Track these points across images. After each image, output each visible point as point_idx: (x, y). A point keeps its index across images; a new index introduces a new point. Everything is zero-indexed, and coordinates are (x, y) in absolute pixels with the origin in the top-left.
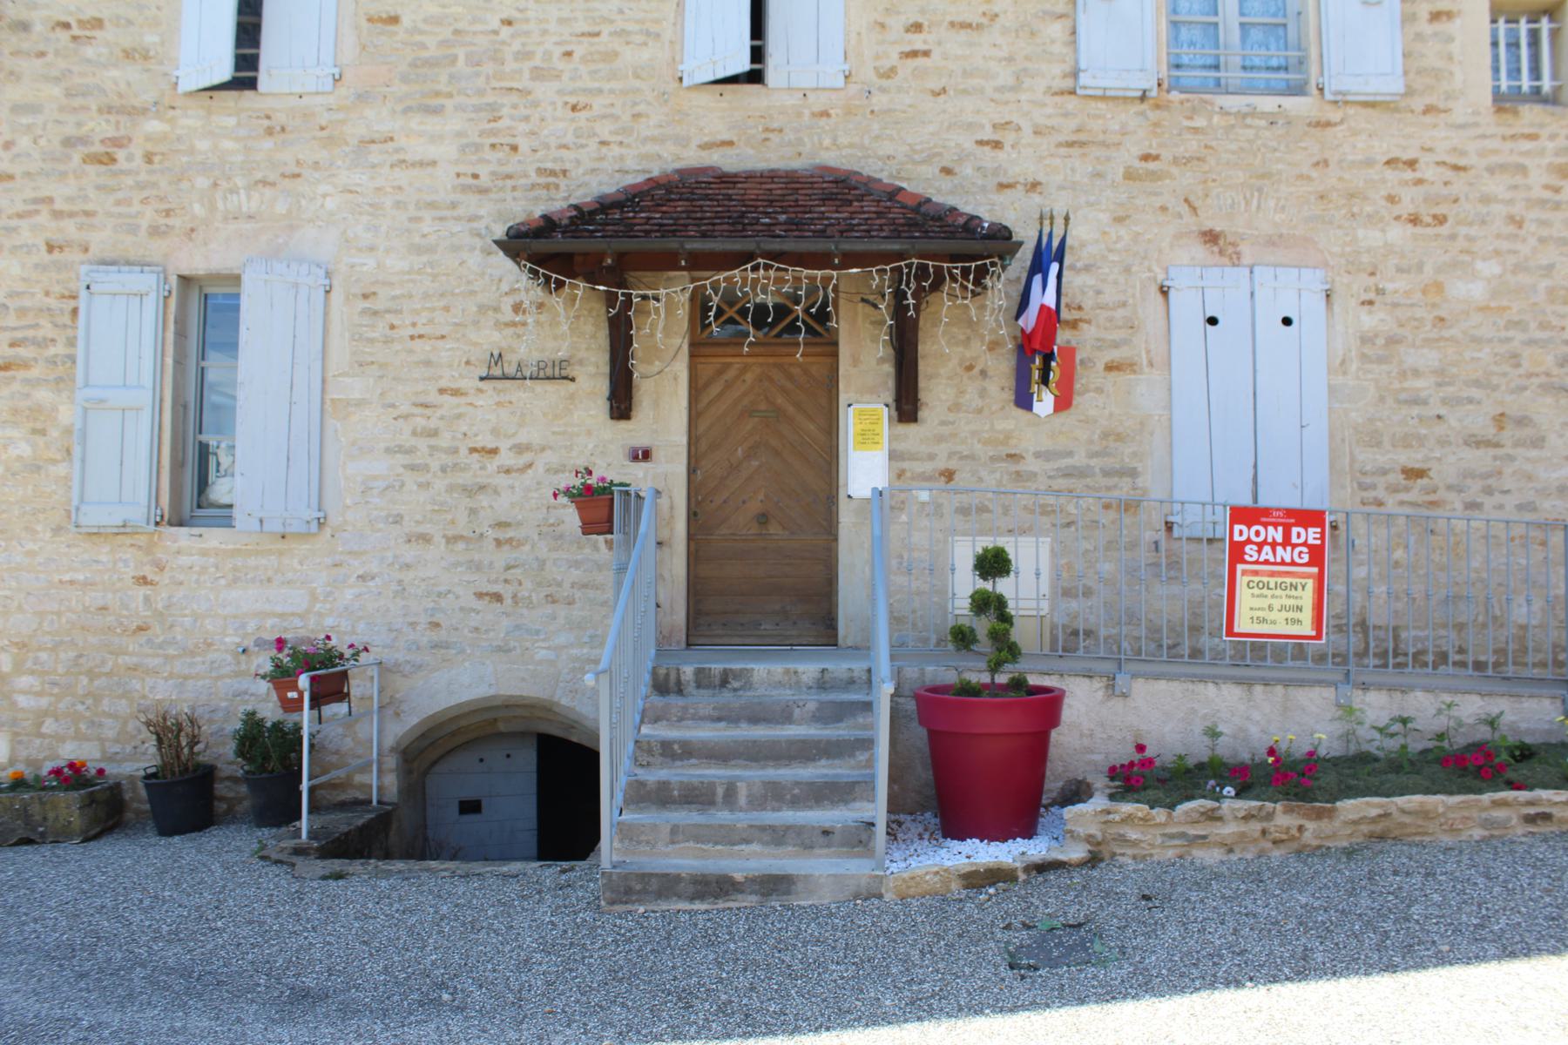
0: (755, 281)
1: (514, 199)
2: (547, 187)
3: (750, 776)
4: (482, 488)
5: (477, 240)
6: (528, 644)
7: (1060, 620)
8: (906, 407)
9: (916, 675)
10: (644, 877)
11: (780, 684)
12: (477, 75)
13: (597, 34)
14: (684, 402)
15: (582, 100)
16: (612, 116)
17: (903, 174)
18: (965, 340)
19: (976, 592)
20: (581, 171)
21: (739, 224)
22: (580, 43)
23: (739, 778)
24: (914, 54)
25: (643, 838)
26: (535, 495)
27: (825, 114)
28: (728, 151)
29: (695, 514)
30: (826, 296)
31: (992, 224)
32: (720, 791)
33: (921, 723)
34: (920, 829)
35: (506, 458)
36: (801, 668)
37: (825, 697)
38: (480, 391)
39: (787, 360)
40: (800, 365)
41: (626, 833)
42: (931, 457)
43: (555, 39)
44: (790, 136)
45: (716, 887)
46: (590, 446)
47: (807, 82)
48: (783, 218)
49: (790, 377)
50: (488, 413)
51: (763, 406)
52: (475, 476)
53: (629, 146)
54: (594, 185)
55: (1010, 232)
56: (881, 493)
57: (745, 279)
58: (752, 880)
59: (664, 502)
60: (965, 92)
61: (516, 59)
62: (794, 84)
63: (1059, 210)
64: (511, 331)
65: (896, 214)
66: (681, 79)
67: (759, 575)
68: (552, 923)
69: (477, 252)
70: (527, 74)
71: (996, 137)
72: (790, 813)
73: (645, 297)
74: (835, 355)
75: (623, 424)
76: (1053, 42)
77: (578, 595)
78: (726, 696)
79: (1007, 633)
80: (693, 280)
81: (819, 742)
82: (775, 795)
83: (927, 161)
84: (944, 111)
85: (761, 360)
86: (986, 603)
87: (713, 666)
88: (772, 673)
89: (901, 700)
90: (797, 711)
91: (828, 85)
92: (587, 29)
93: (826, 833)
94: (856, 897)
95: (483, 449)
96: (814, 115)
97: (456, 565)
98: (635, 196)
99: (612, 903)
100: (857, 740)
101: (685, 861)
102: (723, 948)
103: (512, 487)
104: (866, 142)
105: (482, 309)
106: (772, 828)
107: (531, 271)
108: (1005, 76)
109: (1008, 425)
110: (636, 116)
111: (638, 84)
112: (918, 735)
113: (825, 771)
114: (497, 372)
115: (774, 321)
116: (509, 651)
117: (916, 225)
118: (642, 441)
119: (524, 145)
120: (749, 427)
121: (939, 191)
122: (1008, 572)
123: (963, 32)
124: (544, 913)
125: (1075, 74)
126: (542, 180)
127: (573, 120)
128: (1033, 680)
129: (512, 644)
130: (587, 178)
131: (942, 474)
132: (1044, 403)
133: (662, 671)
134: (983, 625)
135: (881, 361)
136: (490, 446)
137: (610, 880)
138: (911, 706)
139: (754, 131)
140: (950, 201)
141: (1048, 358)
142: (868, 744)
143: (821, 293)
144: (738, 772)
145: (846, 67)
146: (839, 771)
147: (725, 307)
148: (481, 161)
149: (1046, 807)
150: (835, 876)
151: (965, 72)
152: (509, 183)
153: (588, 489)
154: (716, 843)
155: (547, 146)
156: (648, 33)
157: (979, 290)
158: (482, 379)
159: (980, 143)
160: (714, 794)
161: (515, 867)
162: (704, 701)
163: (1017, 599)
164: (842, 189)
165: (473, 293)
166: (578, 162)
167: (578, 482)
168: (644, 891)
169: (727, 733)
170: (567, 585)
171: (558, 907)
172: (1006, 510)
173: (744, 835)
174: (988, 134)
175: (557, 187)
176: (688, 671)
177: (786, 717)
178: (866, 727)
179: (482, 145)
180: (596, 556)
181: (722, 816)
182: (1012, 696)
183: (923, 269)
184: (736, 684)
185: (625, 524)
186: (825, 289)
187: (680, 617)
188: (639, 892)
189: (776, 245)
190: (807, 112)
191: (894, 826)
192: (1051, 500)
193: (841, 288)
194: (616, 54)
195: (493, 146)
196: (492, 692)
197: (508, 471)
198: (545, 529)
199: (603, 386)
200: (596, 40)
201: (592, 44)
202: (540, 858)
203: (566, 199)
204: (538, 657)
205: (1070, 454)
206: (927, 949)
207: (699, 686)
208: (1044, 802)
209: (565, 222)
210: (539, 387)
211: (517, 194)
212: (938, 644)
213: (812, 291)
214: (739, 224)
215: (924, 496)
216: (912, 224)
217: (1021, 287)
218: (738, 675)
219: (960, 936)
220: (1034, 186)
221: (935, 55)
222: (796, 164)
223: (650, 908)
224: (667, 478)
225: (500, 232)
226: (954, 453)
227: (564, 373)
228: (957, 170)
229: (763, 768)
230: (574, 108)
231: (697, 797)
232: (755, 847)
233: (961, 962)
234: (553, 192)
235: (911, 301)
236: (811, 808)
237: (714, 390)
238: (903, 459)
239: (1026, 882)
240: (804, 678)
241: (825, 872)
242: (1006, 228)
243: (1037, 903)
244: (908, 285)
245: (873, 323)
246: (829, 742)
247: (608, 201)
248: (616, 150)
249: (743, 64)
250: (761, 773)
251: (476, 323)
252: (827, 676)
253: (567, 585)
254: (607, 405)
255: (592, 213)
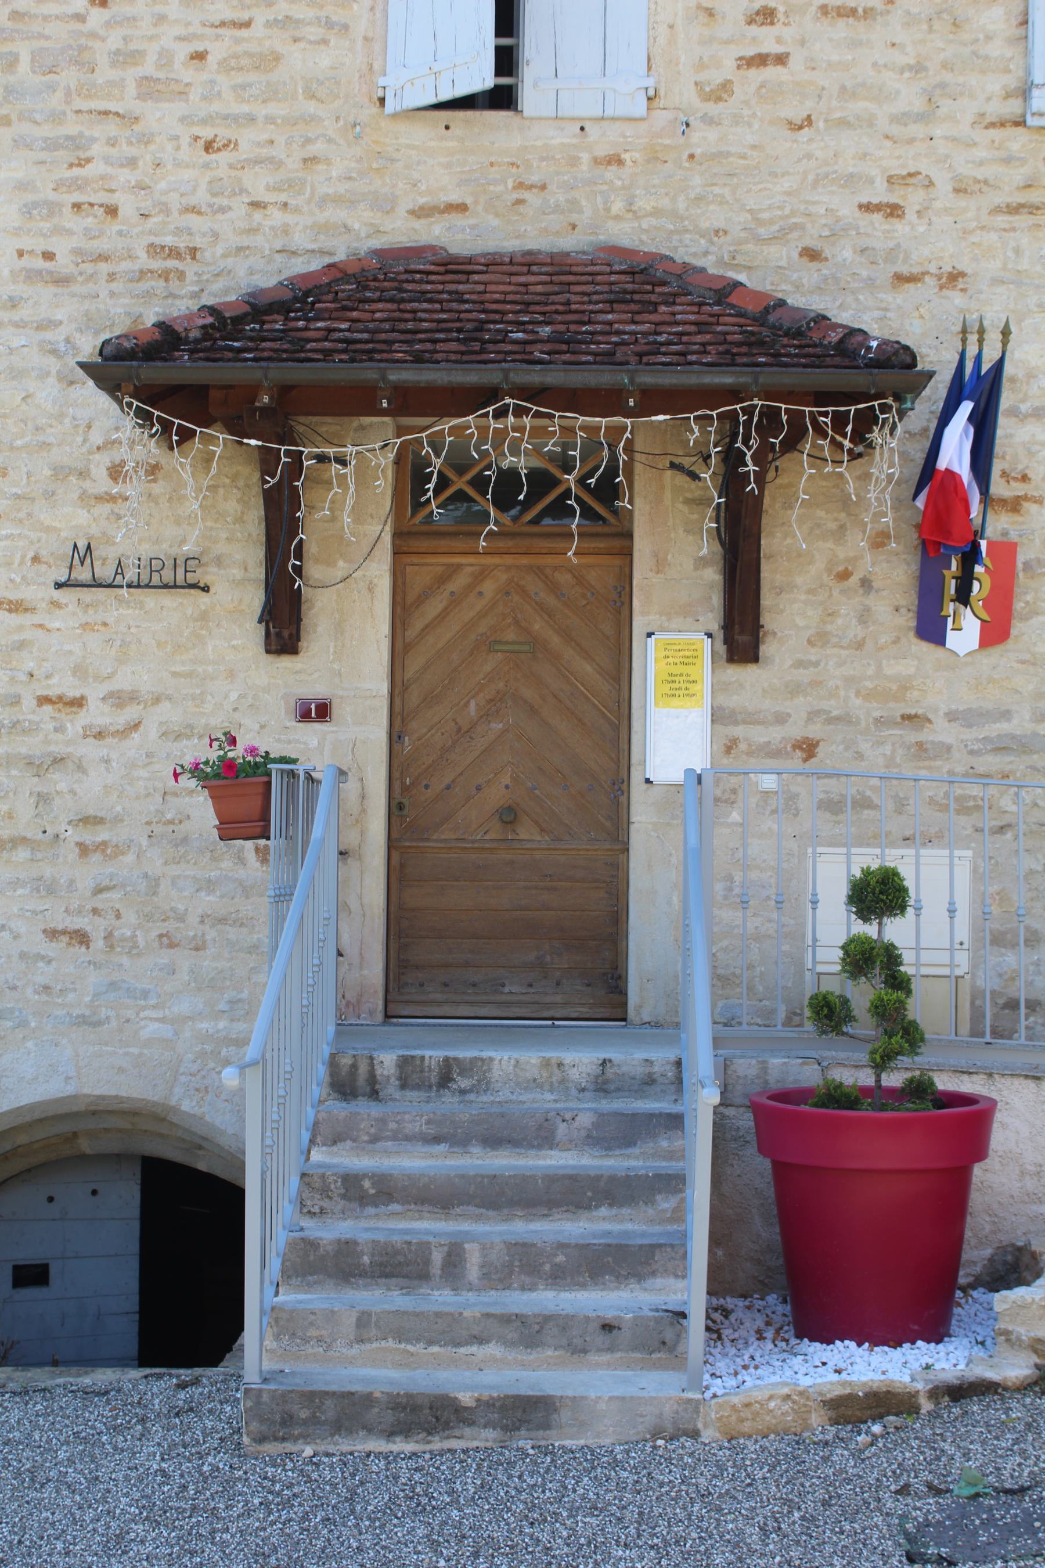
0: (501, 435)
1: (112, 294)
2: (165, 275)
3: (487, 1233)
4: (58, 761)
5: (52, 359)
6: (130, 1014)
7: (988, 982)
8: (742, 639)
9: (753, 1072)
10: (312, 1398)
11: (535, 1084)
12: (52, 88)
13: (247, 24)
14: (385, 628)
15: (223, 133)
16: (271, 160)
17: (740, 260)
18: (836, 529)
19: (852, 941)
20: (219, 251)
21: (475, 340)
22: (218, 37)
23: (471, 1237)
24: (761, 60)
25: (313, 1332)
26: (143, 773)
27: (617, 160)
28: (458, 220)
29: (401, 807)
30: (613, 458)
31: (884, 343)
32: (437, 1257)
33: (762, 1150)
34: (760, 1323)
35: (97, 714)
36: (569, 1057)
37: (607, 1105)
38: (55, 604)
39: (549, 560)
40: (570, 569)
41: (283, 1322)
42: (781, 719)
43: (179, 30)
44: (558, 196)
45: (429, 1415)
46: (234, 696)
47: (586, 106)
48: (546, 331)
49: (554, 588)
50: (68, 638)
51: (510, 635)
52: (47, 742)
53: (297, 210)
54: (242, 273)
55: (914, 357)
56: (699, 778)
57: (483, 430)
58: (486, 1405)
59: (351, 786)
60: (843, 123)
61: (114, 64)
62: (565, 111)
63: (993, 318)
64: (105, 508)
65: (728, 325)
66: (382, 101)
67: (501, 910)
68: (164, 1473)
69: (52, 380)
70: (131, 89)
71: (893, 199)
72: (550, 1294)
73: (322, 459)
74: (627, 553)
75: (286, 662)
76: (989, 38)
77: (211, 934)
78: (448, 1103)
79: (901, 1006)
80: (400, 432)
81: (598, 1178)
82: (525, 1264)
83: (779, 237)
84: (809, 156)
85: (509, 560)
86: (867, 959)
87: (427, 1053)
88: (526, 1064)
89: (730, 1112)
90: (562, 1128)
91: (620, 112)
92: (229, 15)
93: (607, 1327)
94: (656, 1435)
95: (60, 698)
96: (596, 161)
97: (16, 883)
98: (307, 294)
99: (261, 1439)
100: (657, 1176)
101: (379, 1371)
102: (440, 1517)
103: (107, 761)
104: (681, 205)
105: (60, 473)
106: (521, 1319)
107: (140, 413)
108: (909, 97)
109: (904, 668)
110: (310, 161)
111: (312, 107)
112: (757, 1169)
113: (608, 1226)
114: (83, 574)
115: (527, 496)
116: (99, 1023)
117: (762, 343)
118: (317, 690)
119: (128, 205)
120: (488, 668)
121: (798, 287)
122: (903, 908)
123: (841, 23)
124: (149, 1456)
125: (1025, 92)
126: (157, 264)
127: (206, 166)
128: (944, 1083)
129: (103, 1013)
130: (230, 261)
131: (797, 746)
132: (965, 632)
133: (346, 1061)
134: (862, 995)
135: (701, 563)
136: (72, 693)
137: (258, 1403)
138: (746, 1121)
139: (499, 188)
140: (817, 304)
141: (971, 556)
142: (674, 1183)
143: (606, 452)
144: (465, 1226)
145: (650, 82)
146: (629, 1226)
147: (451, 474)
148: (59, 231)
149: (963, 1289)
150: (623, 1399)
151: (843, 89)
152: (104, 268)
153: (229, 767)
154: (430, 1343)
155: (165, 209)
156: (329, 24)
157: (860, 449)
158: (59, 586)
159: (867, 208)
160: (427, 1262)
161: (103, 1377)
162: (413, 1109)
163: (918, 949)
164: (641, 283)
165: (45, 445)
166: (216, 235)
167: (214, 755)
168: (313, 1421)
169: (451, 1162)
170: (193, 919)
171: (173, 1445)
172: (901, 806)
173: (476, 1330)
174: (879, 194)
175: (181, 275)
176: (387, 1061)
177: (543, 1137)
178: (671, 1155)
179: (61, 205)
180: (242, 873)
181: (441, 1298)
182: (908, 1110)
183: (771, 415)
184: (464, 1083)
185: (288, 822)
186: (612, 447)
187: (374, 972)
188: (305, 1422)
189: (534, 377)
190: (585, 157)
191: (717, 1316)
192: (975, 790)
193: (638, 446)
194: (277, 58)
195: (77, 206)
196: (70, 1090)
197: (100, 735)
198: (158, 829)
199: (255, 599)
200: (244, 33)
201: (238, 41)
202: (143, 1361)
203: (195, 295)
204: (145, 1034)
205: (1006, 715)
206: (771, 1524)
207: (403, 1086)
208: (962, 1280)
209: (194, 334)
210: (151, 599)
211: (117, 286)
212: (788, 1022)
213: (591, 448)
214: (475, 340)
215: (769, 782)
216: (754, 343)
217: (927, 444)
218: (467, 1067)
219: (825, 1503)
220: (954, 277)
221: (796, 62)
222: (568, 243)
223: (322, 1448)
224: (353, 753)
225: (88, 348)
226: (818, 712)
227: (191, 578)
228: (827, 253)
229: (508, 1219)
230: (208, 147)
231: (400, 1266)
232: (493, 1350)
233: (828, 1549)
234: (174, 285)
235: (751, 467)
236: (583, 1286)
237: (434, 607)
238: (736, 723)
239: (934, 1415)
240: (574, 1074)
241: (606, 1390)
242: (906, 348)
243: (950, 1449)
244: (746, 442)
245: (688, 502)
246: (613, 1179)
247: (265, 300)
248: (277, 217)
249: (482, 77)
250: (503, 1227)
251: (50, 495)
252: (610, 1072)
253: (193, 919)
254: (261, 629)
255: (239, 320)
